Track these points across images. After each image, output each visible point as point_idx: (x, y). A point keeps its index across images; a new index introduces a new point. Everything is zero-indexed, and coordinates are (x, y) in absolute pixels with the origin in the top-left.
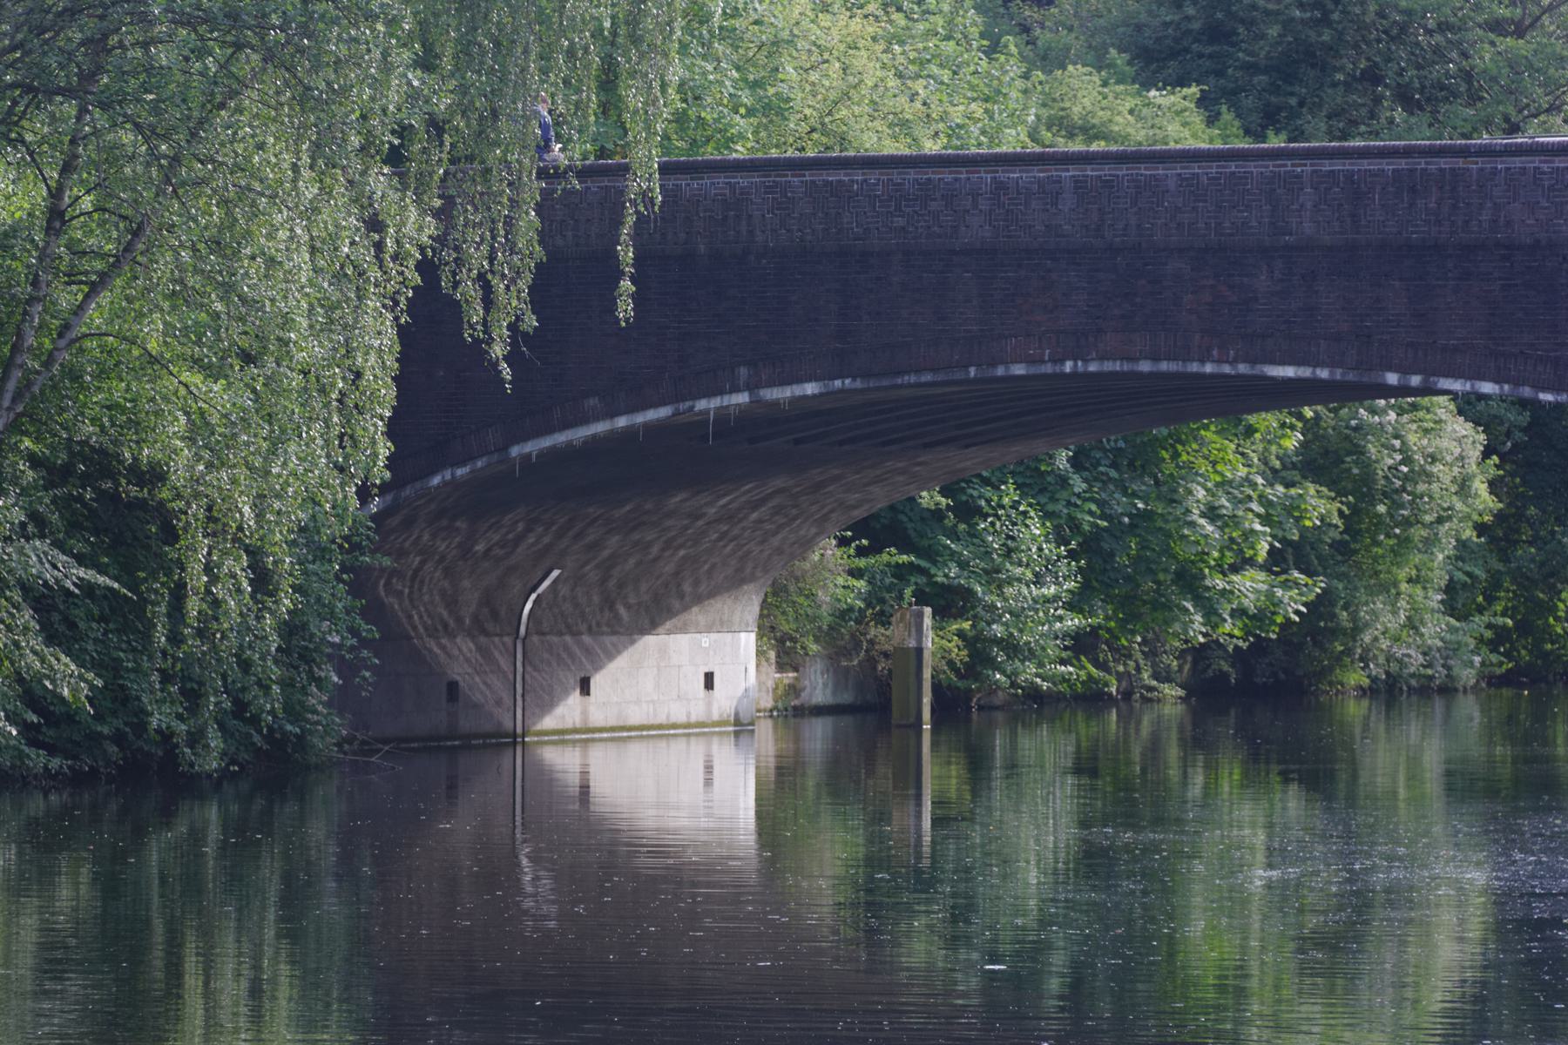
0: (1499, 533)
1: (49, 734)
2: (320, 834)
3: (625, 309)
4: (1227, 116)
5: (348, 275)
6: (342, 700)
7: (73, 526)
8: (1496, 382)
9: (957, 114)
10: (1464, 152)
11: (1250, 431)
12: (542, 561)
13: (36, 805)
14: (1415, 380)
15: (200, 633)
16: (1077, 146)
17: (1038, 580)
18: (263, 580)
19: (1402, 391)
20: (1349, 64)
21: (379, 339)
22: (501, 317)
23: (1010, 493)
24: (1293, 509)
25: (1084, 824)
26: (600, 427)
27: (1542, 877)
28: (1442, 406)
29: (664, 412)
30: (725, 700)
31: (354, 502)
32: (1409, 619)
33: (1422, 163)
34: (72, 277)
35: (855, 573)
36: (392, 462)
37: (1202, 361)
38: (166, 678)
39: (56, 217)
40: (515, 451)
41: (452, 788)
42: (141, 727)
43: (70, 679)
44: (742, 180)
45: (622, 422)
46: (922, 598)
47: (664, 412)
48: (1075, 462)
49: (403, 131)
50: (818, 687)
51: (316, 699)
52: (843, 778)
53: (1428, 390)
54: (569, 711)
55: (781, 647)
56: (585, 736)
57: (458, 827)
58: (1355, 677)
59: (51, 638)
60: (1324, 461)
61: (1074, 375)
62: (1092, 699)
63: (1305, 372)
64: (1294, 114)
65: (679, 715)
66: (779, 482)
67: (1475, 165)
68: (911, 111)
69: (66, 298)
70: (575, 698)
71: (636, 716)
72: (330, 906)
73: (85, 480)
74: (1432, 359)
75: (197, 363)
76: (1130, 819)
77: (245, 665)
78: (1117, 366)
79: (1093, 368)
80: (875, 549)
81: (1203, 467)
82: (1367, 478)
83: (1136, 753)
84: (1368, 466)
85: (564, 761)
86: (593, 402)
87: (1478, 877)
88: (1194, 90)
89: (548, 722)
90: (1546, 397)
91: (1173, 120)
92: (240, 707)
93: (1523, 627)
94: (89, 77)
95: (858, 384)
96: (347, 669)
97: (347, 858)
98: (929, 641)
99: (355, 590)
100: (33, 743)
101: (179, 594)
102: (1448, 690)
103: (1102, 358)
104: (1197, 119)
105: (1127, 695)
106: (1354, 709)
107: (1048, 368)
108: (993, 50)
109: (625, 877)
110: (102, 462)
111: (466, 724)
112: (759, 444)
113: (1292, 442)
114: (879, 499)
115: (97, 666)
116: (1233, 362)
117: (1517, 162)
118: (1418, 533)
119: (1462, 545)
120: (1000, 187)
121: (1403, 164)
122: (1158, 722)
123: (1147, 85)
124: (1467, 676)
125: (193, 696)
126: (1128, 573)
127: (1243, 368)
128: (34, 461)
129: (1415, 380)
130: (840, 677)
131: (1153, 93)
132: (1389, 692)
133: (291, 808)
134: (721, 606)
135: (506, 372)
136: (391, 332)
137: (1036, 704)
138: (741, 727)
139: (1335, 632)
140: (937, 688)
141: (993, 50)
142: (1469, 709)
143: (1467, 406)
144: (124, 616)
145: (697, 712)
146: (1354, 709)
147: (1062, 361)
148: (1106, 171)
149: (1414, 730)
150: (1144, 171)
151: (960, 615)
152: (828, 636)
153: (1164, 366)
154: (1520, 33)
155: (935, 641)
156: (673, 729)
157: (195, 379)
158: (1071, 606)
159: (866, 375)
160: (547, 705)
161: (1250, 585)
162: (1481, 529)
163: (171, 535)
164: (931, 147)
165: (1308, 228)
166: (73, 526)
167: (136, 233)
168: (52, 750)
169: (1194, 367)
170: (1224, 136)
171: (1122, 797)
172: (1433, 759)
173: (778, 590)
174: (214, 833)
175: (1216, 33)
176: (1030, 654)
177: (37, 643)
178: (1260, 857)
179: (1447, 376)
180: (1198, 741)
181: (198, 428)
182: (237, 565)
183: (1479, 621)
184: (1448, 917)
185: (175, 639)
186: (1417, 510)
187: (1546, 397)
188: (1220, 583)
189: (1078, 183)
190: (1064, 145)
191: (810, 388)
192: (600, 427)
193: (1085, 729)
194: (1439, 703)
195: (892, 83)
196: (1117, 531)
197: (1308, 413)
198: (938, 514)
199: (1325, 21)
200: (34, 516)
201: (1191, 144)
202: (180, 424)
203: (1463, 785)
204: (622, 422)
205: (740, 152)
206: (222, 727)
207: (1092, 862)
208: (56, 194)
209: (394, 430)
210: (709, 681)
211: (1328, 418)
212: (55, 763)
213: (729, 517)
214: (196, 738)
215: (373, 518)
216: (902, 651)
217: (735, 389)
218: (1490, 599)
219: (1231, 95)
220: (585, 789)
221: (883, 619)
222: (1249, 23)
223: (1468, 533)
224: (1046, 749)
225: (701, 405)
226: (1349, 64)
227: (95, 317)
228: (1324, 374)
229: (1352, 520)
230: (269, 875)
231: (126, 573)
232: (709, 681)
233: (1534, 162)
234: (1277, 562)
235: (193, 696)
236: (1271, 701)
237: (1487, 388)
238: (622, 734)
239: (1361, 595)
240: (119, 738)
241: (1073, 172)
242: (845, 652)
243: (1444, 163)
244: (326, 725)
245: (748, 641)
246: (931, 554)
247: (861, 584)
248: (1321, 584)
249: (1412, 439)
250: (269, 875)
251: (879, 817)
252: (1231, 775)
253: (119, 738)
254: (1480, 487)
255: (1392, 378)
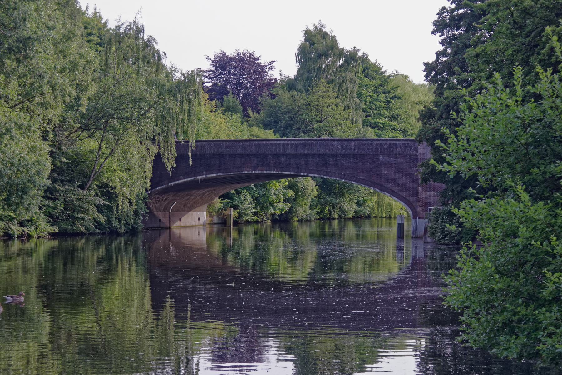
0: (318, 197)
1: (98, 227)
2: (140, 242)
3: (191, 163)
4: (277, 134)
5: (145, 158)
6: (143, 222)
7: (102, 195)
9: (237, 134)
10: (313, 140)
11: (280, 182)
12: (174, 200)
13: (97, 237)
14: (306, 174)
15: (121, 212)
16: (255, 138)
17: (249, 204)
18: (131, 203)
19: (304, 176)
20: (295, 127)
21: (149, 166)
22: (170, 164)
23: (245, 191)
24: (287, 194)
25: (256, 241)
26: (183, 181)
28: (309, 178)
29: (192, 178)
30: (201, 222)
31: (144, 192)
32: (304, 210)
33: (307, 142)
34: (102, 157)
35: (221, 203)
36: (150, 186)
38: (116, 218)
39: (100, 148)
40: (170, 184)
41: (160, 235)
42: (112, 226)
43: (102, 219)
44: (204, 143)
45: (186, 180)
46: (231, 207)
47: (192, 178)
48: (255, 186)
49: (154, 136)
50: (216, 220)
51: (139, 221)
52: (219, 234)
53: (307, 176)
54: (178, 223)
55: (210, 215)
56: (180, 227)
58: (296, 219)
59: (99, 212)
60: (291, 187)
61: (254, 173)
62: (257, 222)
63: (289, 173)
64: (287, 134)
65: (194, 224)
66: (209, 189)
67: (314, 142)
68: (230, 133)
69: (102, 160)
70: (179, 222)
71: (188, 224)
72: (141, 254)
73: (104, 188)
74: (308, 171)
75: (121, 170)
76: (262, 241)
77: (128, 216)
78: (260, 172)
80: (224, 199)
81: (274, 187)
82: (298, 189)
83: (263, 231)
84: (298, 187)
85: (177, 231)
86: (181, 177)
87: (314, 249)
88: (272, 130)
89: (174, 225)
90: (325, 177)
91: (269, 135)
92: (127, 222)
93: (321, 212)
94: (105, 127)
96: (144, 216)
97: (144, 246)
98: (232, 214)
99: (146, 205)
100: (96, 228)
101: (118, 206)
102: (310, 221)
104: (273, 134)
105: (262, 222)
106: (296, 224)
108: (242, 124)
109: (183, 247)
110: (107, 186)
111: (162, 226)
112: (206, 183)
113: (287, 183)
114: (225, 191)
115: (106, 217)
117: (321, 142)
118: (306, 197)
119: (312, 199)
120: (243, 145)
121: (304, 142)
122: (266, 226)
123: (265, 130)
124: (313, 219)
125: (120, 221)
126: (261, 203)
127: (280, 172)
128: (96, 185)
129: (306, 174)
130: (219, 218)
132: (301, 221)
133: (135, 238)
134: (200, 208)
135: (171, 173)
136: (151, 166)
137: (248, 223)
138: (204, 225)
139: (293, 212)
140: (233, 220)
141: (242, 124)
142: (313, 224)
143: (313, 178)
144: (110, 208)
145: (197, 224)
146: (296, 224)
148: (259, 142)
149: (305, 227)
150: (265, 142)
151: (237, 209)
152: (217, 212)
153: (268, 172)
154: (321, 122)
155: (234, 214)
156: (194, 226)
157: (121, 173)
158: (254, 208)
159: (223, 173)
160: (174, 223)
161: (281, 205)
162: (315, 197)
163: (117, 197)
164: (233, 139)
165: (289, 151)
166: (102, 195)
167: (112, 151)
168: (99, 229)
169: (272, 172)
170: (277, 137)
171: (262, 237)
172: (308, 231)
173: (210, 205)
174: (123, 242)
175: (276, 122)
176: (247, 215)
177: (97, 213)
178: (282, 246)
180: (273, 228)
181: (121, 180)
182: (126, 202)
183: (315, 211)
184: (310, 256)
185: (117, 212)
186: (305, 194)
187: (325, 177)
188: (276, 204)
189: (255, 144)
190: (253, 138)
191: (215, 175)
192: (183, 181)
193: (256, 226)
194: (309, 223)
195: (227, 129)
196: (260, 197)
197: (289, 179)
198: (234, 194)
199: (292, 120)
200: (96, 194)
201: (272, 138)
202: (116, 179)
203: (312, 235)
204: (186, 180)
205: (204, 139)
206: (124, 226)
207: (256, 247)
208: (100, 145)
209: (151, 180)
210: (199, 219)
211: (292, 180)
212: (99, 231)
213: (204, 194)
214: (120, 227)
215: (148, 194)
216: (228, 215)
218: (316, 207)
219: (278, 131)
220: (180, 235)
221: (225, 210)
222: (281, 120)
223: (313, 197)
224: (250, 229)
225: (198, 177)
226: (295, 127)
227: (106, 164)
228: (292, 173)
229: (296, 195)
230: (131, 249)
231: (110, 202)
232: (199, 219)
233: (323, 142)
234: (284, 201)
235: (120, 221)
236: (283, 222)
237: (316, 175)
238: (186, 227)
239: (297, 207)
240: (109, 228)
241: (254, 142)
242: (220, 215)
243: (310, 142)
244: (141, 225)
245: (205, 213)
246: (233, 199)
247: (222, 205)
248: (291, 205)
249: (305, 183)
250: (131, 249)
251: (225, 240)
252: (278, 233)
253: (109, 228)
254: (315, 190)
255: (302, 174)
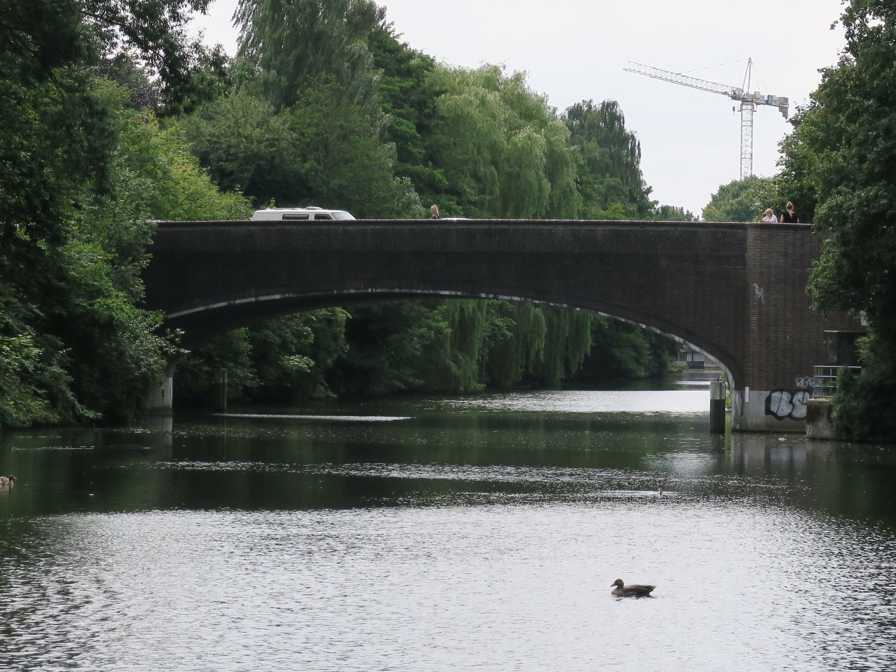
8: (107, 60)
14: (491, 296)
27: (447, 124)
37: (417, 289)
57: (66, 519)
61: (372, 293)
79: (378, 291)
95: (295, 295)
103: (381, 288)
107: (363, 291)
116: (428, 289)
131: (345, 184)
147: (367, 289)
179: (655, 326)
191: (277, 297)
217: (250, 297)
